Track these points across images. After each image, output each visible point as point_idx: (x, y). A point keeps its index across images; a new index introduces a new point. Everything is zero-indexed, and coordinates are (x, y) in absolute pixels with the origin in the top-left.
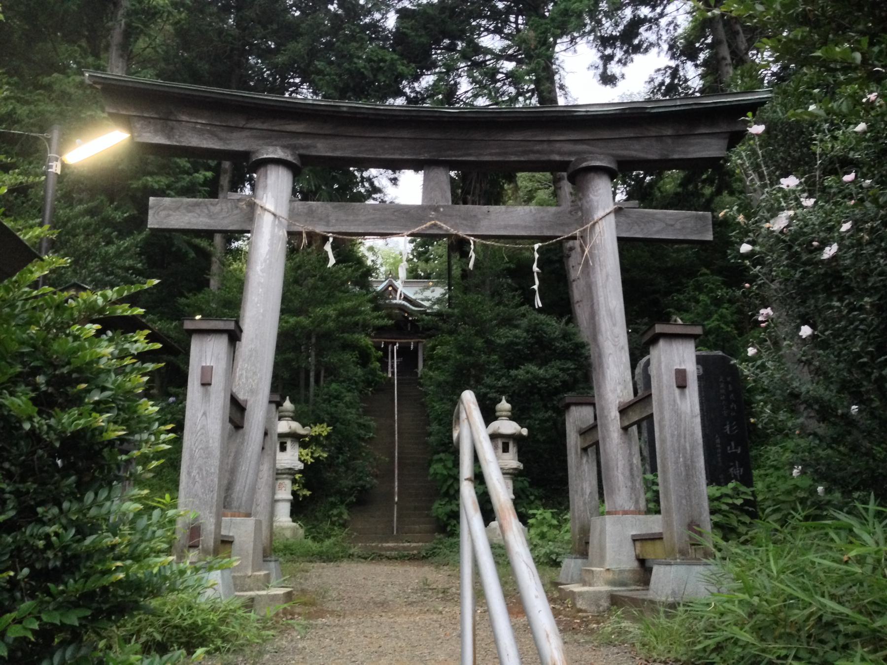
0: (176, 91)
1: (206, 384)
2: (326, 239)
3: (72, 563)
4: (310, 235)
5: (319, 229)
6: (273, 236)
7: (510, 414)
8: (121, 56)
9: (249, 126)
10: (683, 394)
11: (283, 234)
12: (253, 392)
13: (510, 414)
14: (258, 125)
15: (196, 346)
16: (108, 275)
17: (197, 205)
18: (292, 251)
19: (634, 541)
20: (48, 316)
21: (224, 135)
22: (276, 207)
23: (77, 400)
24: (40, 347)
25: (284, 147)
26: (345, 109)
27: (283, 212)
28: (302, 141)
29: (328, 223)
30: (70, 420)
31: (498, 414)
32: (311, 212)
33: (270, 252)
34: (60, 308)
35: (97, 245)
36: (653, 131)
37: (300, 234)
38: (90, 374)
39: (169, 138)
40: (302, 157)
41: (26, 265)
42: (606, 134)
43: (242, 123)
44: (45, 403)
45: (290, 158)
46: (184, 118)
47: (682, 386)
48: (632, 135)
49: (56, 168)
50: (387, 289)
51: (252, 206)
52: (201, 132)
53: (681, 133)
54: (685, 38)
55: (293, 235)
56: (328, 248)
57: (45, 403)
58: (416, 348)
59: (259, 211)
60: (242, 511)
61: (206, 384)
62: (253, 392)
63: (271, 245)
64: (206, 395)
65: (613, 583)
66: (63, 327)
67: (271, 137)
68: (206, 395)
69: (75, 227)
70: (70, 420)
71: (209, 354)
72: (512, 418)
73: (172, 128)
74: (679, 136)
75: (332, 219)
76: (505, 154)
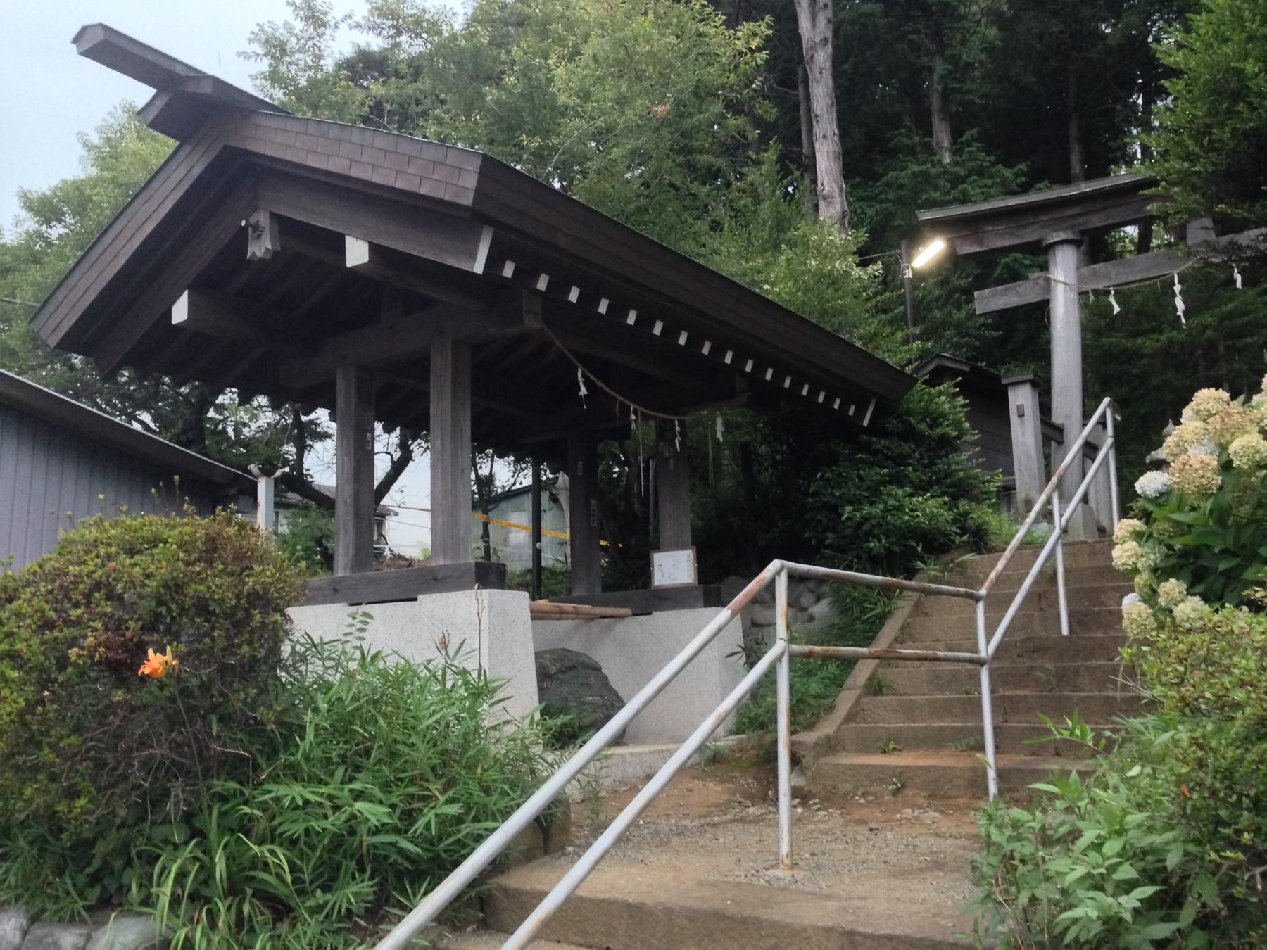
1: (1021, 415)
2: (1108, 292)
3: (948, 475)
4: (1095, 292)
5: (1101, 286)
6: (1066, 301)
8: (944, 119)
11: (1074, 296)
12: (1068, 417)
14: (1044, 218)
16: (963, 337)
17: (1007, 289)
18: (1084, 306)
20: (926, 397)
21: (1019, 233)
22: (1066, 276)
23: (941, 425)
24: (926, 410)
25: (1065, 229)
27: (1072, 280)
28: (1081, 220)
29: (1110, 279)
30: (939, 431)
32: (1095, 274)
33: (1067, 312)
34: (929, 394)
35: (950, 314)
37: (1087, 292)
38: (943, 415)
39: (981, 245)
40: (1082, 233)
43: (1031, 220)
44: (931, 427)
45: (1071, 237)
46: (990, 228)
49: (908, 274)
51: (1048, 280)
52: (1003, 236)
55: (1083, 294)
56: (1112, 299)
57: (931, 427)
59: (1053, 284)
61: (1021, 415)
62: (1068, 417)
63: (1066, 307)
64: (1022, 422)
66: (932, 401)
67: (1055, 225)
68: (1022, 422)
69: (928, 304)
70: (939, 431)
75: (1113, 275)
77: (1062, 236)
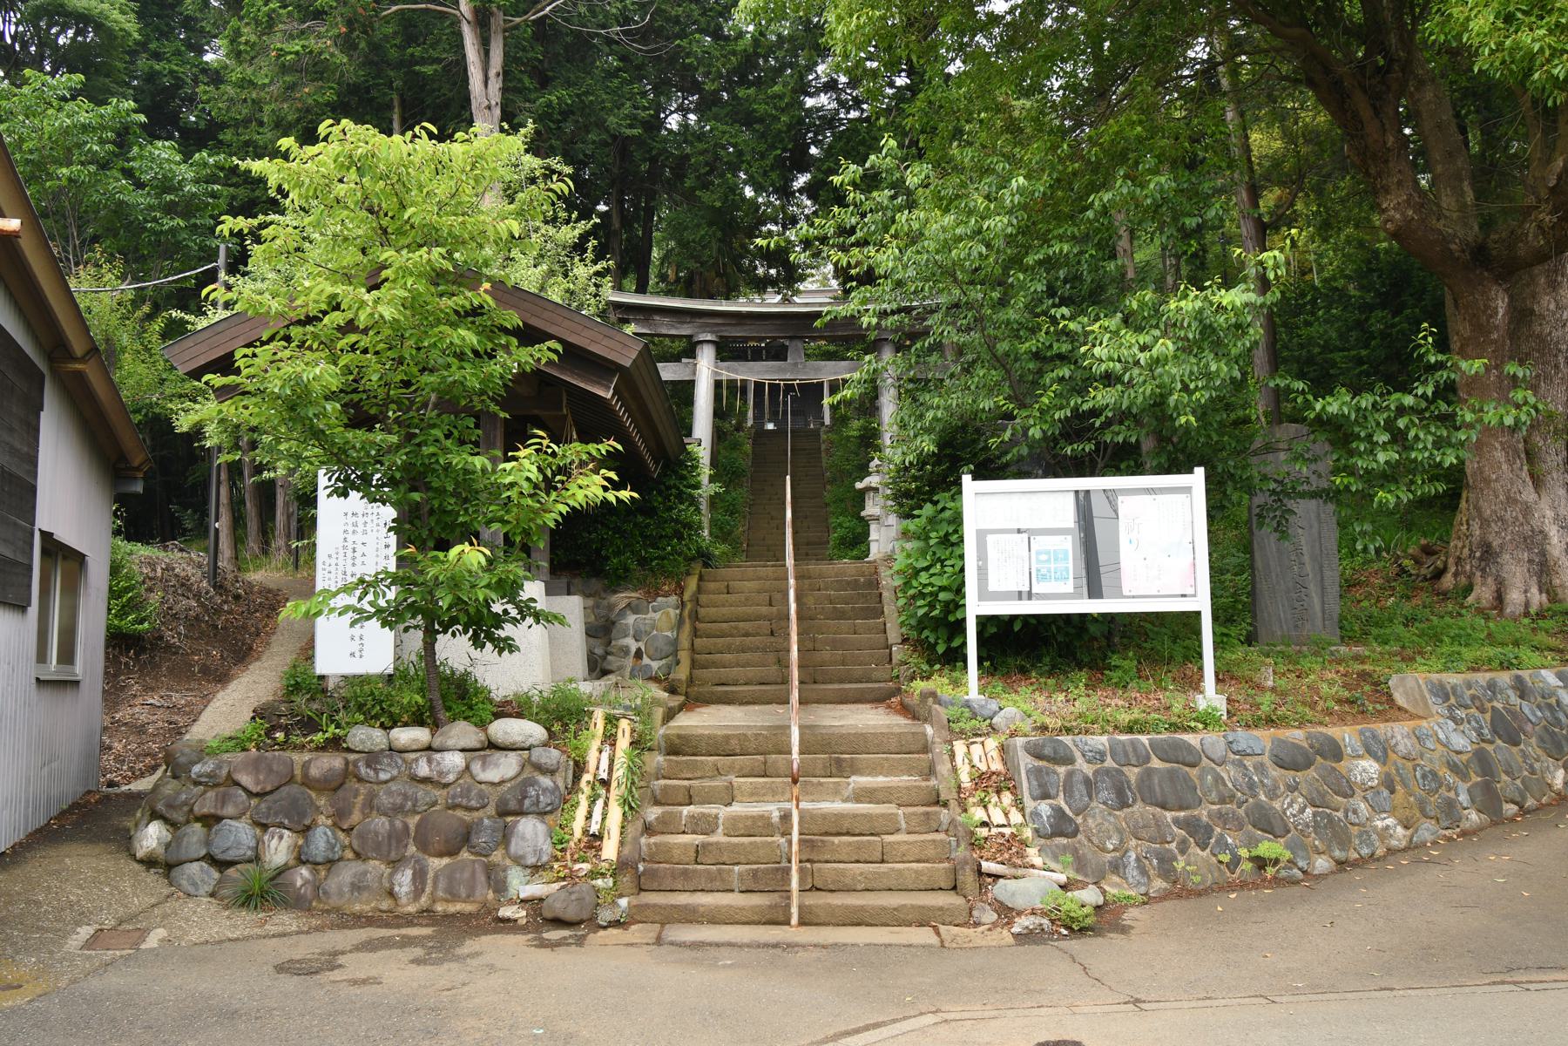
67: (705, 328)
77: (709, 337)
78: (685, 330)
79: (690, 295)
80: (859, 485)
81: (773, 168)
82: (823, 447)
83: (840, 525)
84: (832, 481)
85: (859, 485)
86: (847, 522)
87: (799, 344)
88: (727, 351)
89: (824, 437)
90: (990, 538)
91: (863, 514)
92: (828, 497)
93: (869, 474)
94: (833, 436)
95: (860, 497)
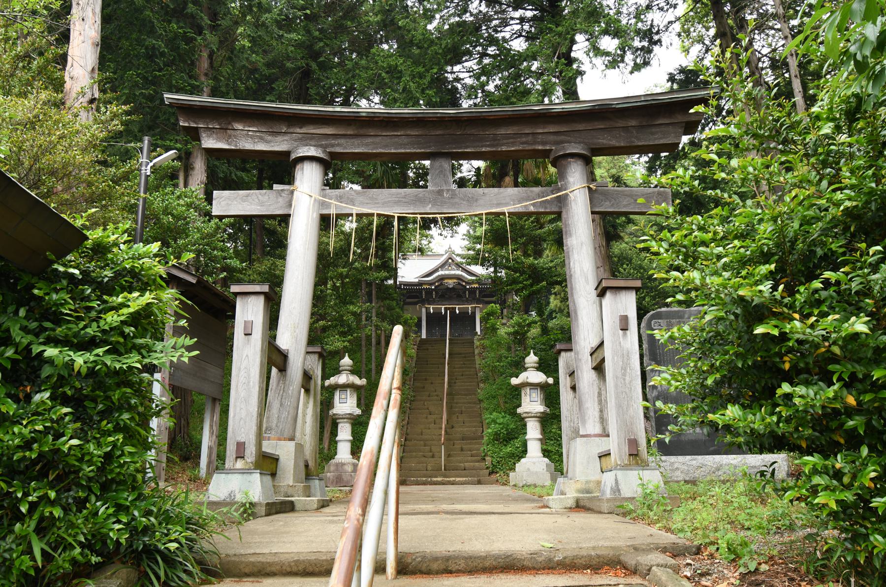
0: (232, 106)
7: (536, 365)
9: (291, 130)
10: (625, 335)
13: (536, 365)
15: (240, 304)
19: (600, 457)
26: (364, 114)
31: (526, 366)
36: (621, 123)
40: (333, 155)
41: (717, 27)
42: (581, 127)
47: (625, 329)
48: (602, 127)
50: (447, 261)
53: (644, 123)
54: (271, 188)
58: (474, 314)
60: (286, 435)
65: (579, 491)
67: (307, 139)
71: (250, 311)
72: (539, 369)
73: (230, 136)
74: (642, 127)
76: (497, 145)
77: (312, 152)
78: (278, 145)
79: (298, 101)
80: (514, 381)
81: (429, 87)
82: (476, 352)
83: (494, 421)
84: (485, 380)
85: (514, 381)
86: (502, 418)
87: (446, 164)
88: (335, 170)
89: (477, 343)
90: (598, 430)
91: (519, 410)
92: (481, 393)
93: (526, 369)
94: (487, 342)
95: (516, 393)
